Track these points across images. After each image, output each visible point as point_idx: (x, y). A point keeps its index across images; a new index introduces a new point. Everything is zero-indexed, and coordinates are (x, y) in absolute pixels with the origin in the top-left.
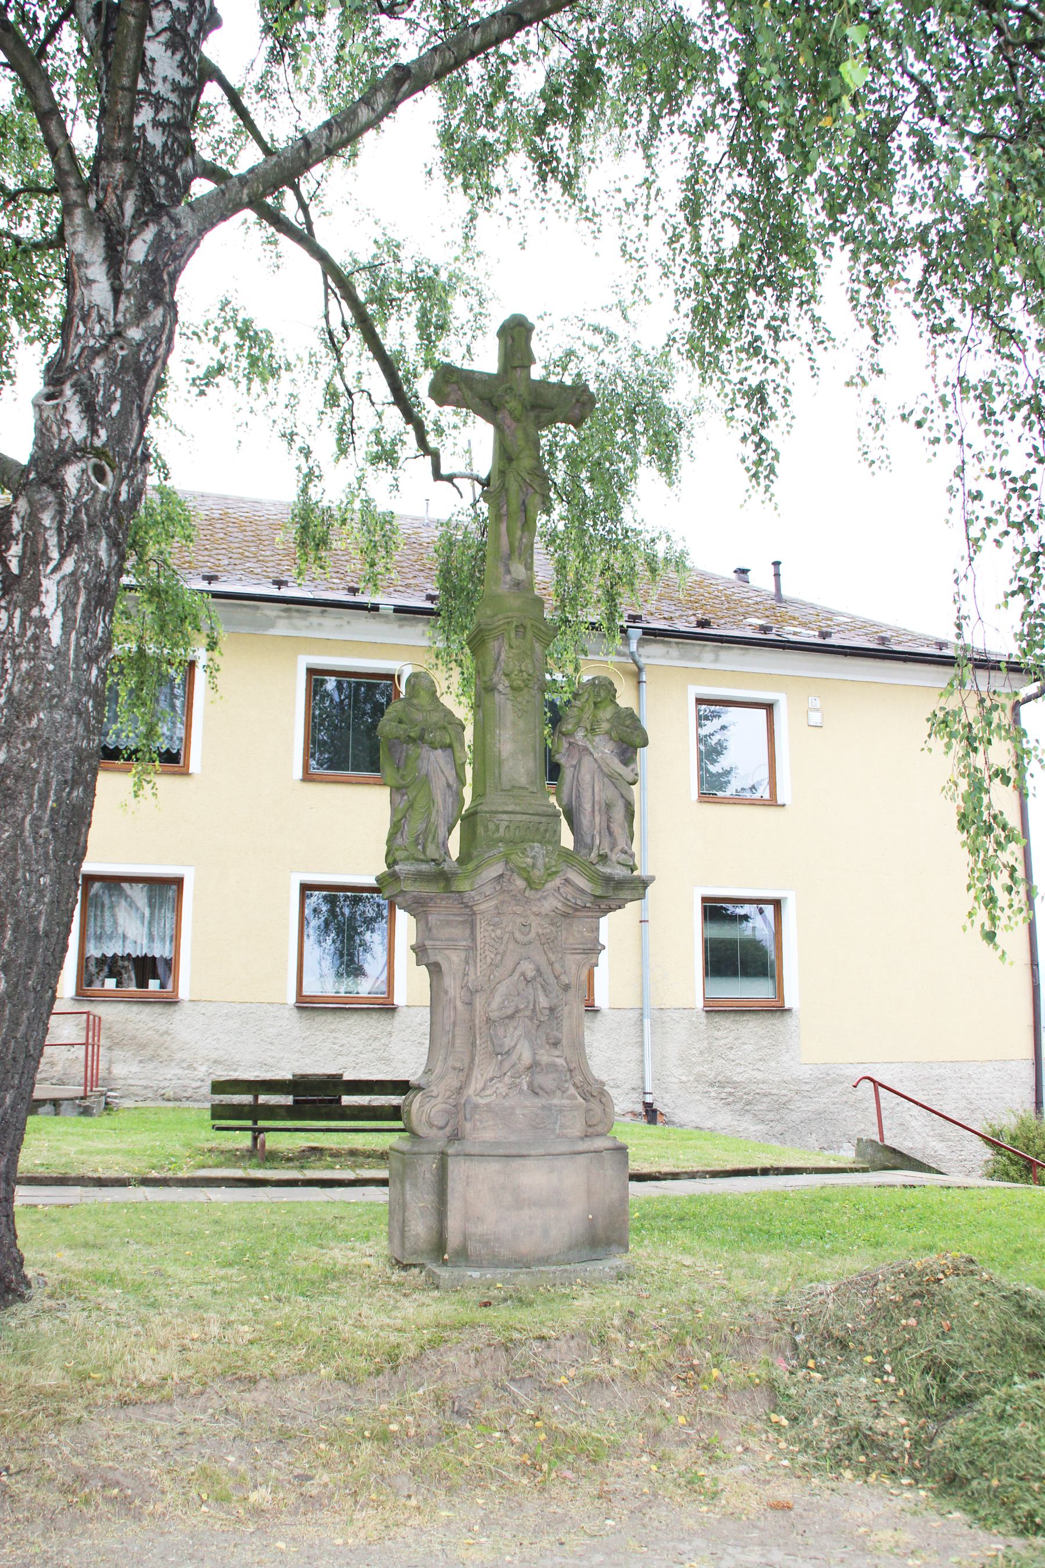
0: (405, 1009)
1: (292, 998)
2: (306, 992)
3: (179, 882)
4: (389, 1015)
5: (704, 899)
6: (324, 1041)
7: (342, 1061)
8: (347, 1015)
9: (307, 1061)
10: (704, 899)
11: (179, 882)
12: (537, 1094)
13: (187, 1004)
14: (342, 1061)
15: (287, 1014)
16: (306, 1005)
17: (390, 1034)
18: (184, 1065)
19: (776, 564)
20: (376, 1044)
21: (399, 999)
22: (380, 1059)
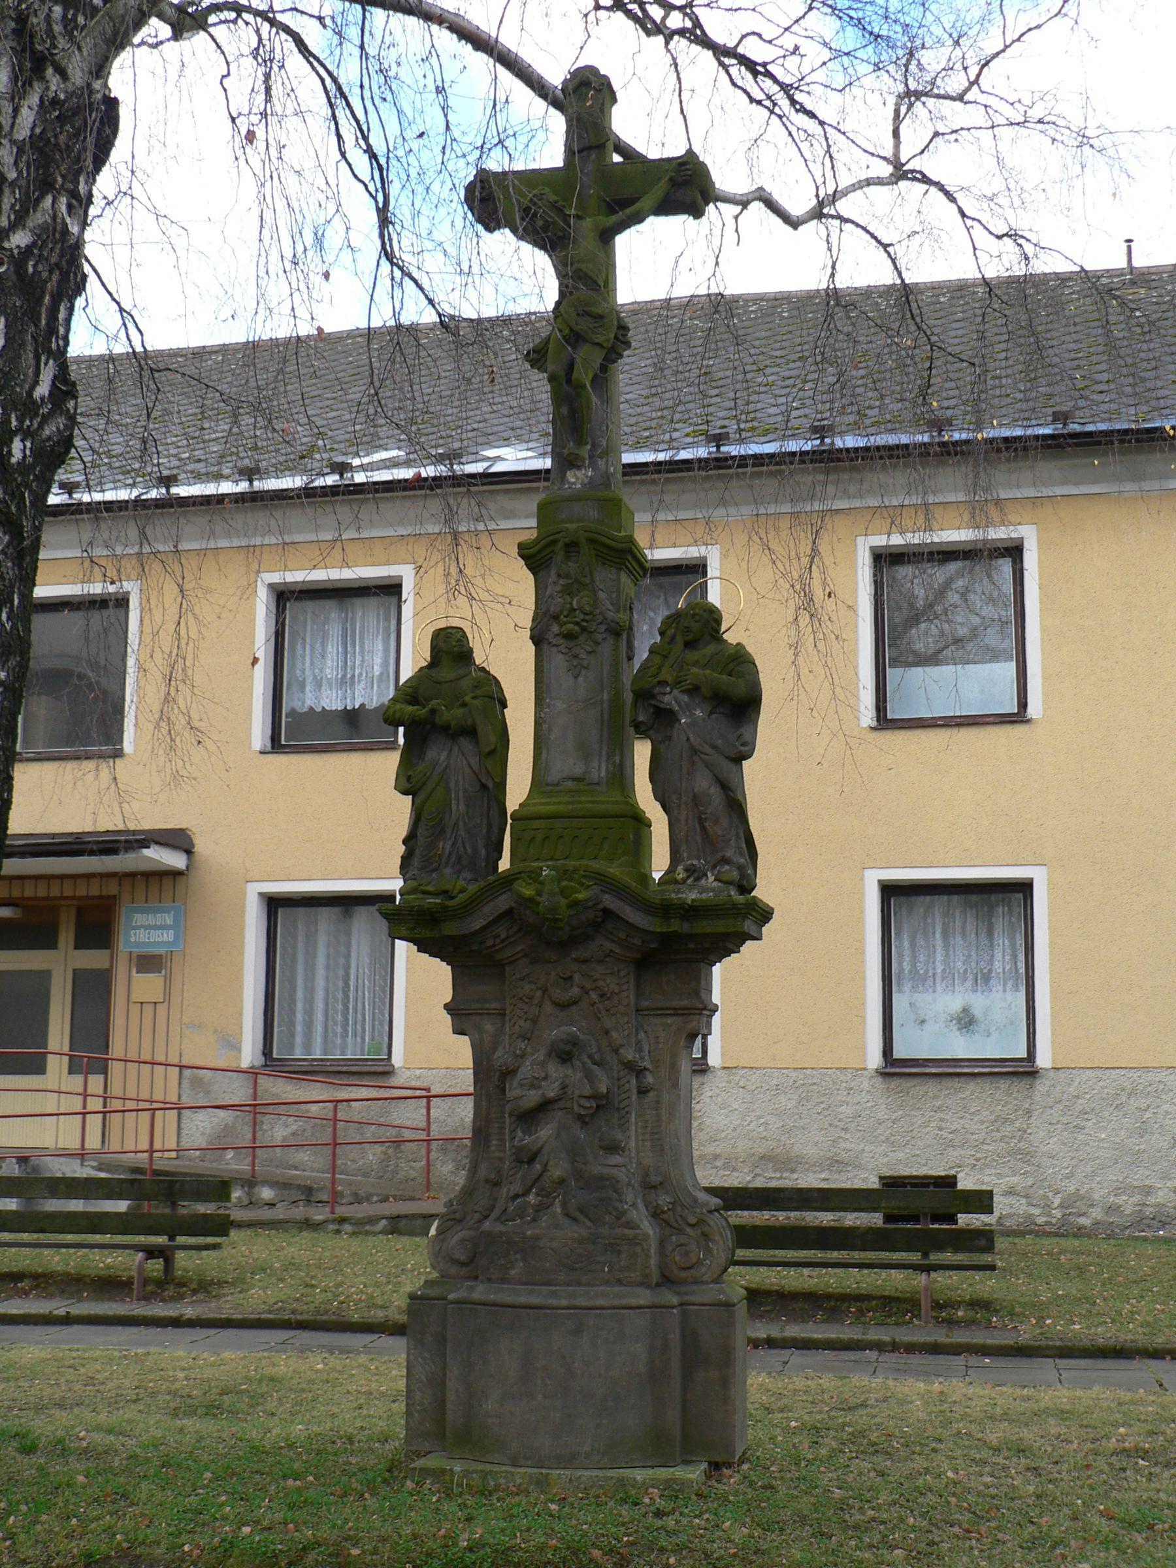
0: (1052, 1074)
1: (874, 1058)
2: (899, 1053)
3: (1024, 888)
4: (1023, 1083)
5: (879, 881)
6: (925, 1125)
7: (954, 1155)
8: (955, 1083)
9: (900, 1155)
10: (879, 881)
11: (1024, 888)
12: (575, 1220)
13: (719, 1073)
14: (954, 1155)
15: (866, 1085)
16: (895, 1068)
17: (1029, 1113)
18: (719, 1164)
19: (1130, 241)
20: (1008, 1129)
21: (1044, 1059)
22: (1013, 1153)
